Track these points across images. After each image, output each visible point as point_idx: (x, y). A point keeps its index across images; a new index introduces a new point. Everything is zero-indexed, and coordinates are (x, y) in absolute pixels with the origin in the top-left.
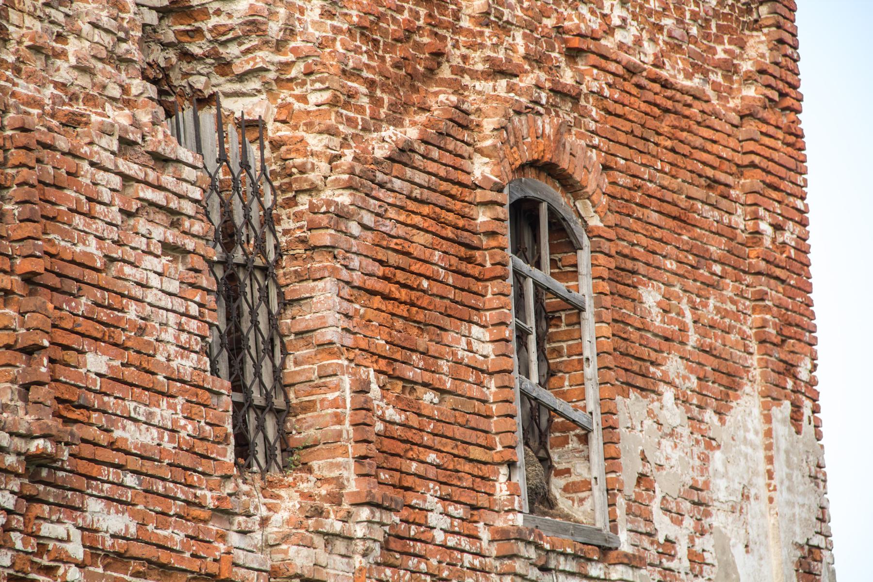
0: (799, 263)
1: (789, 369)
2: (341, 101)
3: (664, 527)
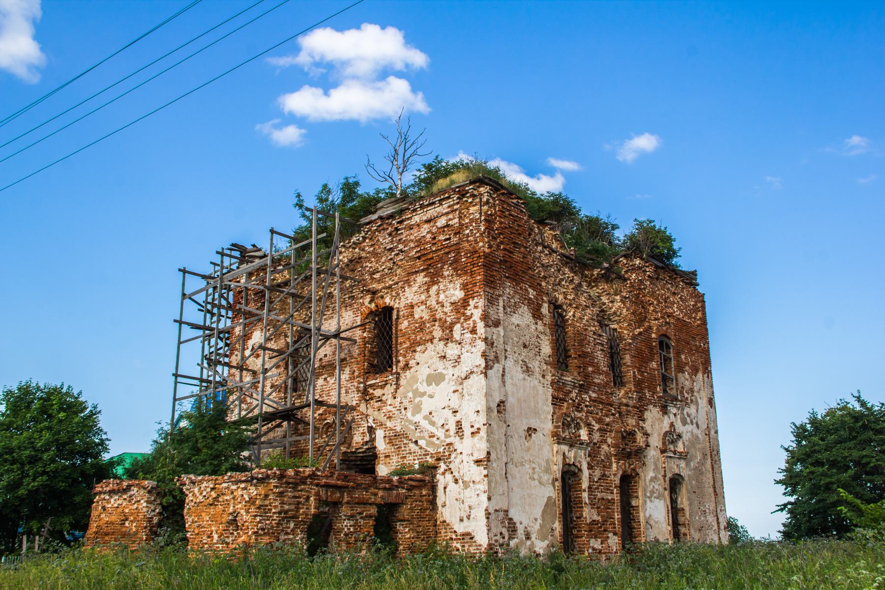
0: (708, 351)
1: (707, 368)
2: (630, 325)
3: (686, 395)
